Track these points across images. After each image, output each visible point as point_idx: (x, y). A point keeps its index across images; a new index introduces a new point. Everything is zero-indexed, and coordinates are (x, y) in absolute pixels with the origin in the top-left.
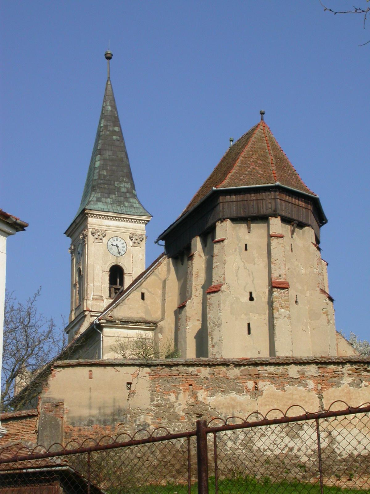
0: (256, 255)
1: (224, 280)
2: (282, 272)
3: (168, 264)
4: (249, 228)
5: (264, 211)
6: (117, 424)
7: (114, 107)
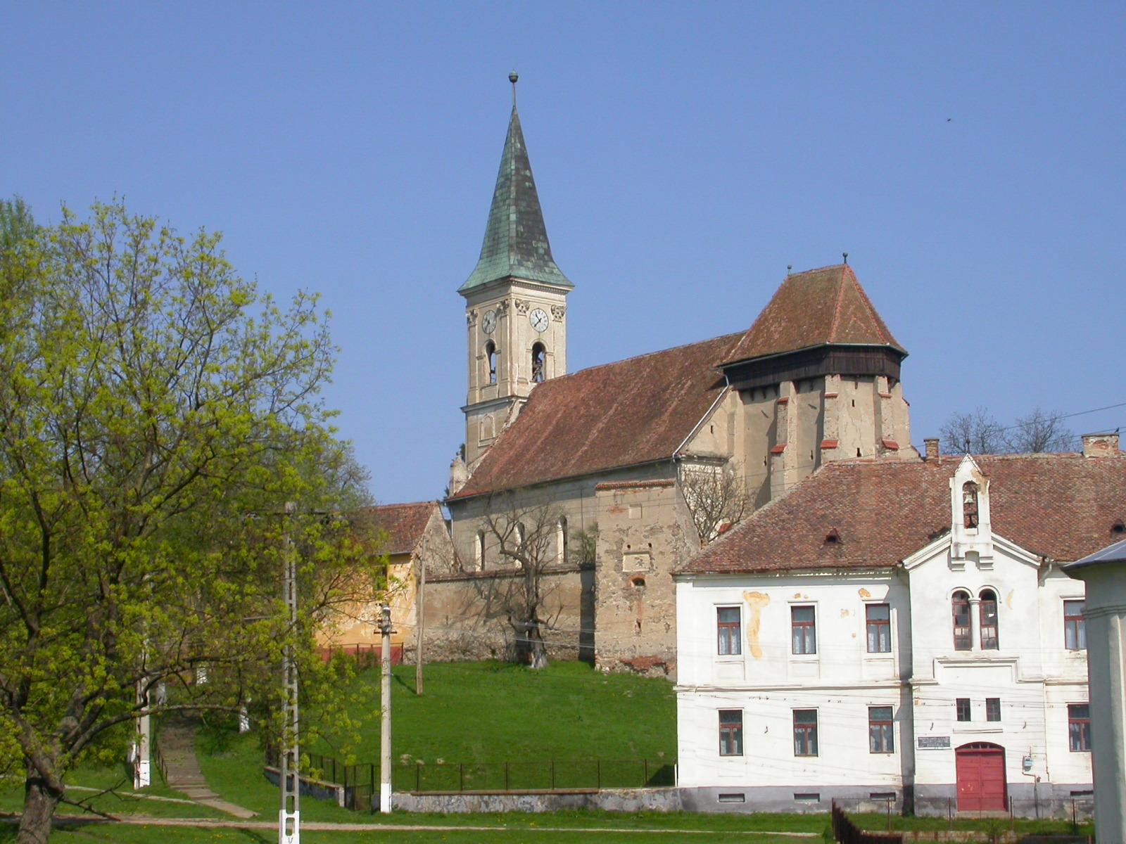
0: (863, 412)
1: (838, 435)
2: (890, 432)
3: (733, 398)
4: (856, 385)
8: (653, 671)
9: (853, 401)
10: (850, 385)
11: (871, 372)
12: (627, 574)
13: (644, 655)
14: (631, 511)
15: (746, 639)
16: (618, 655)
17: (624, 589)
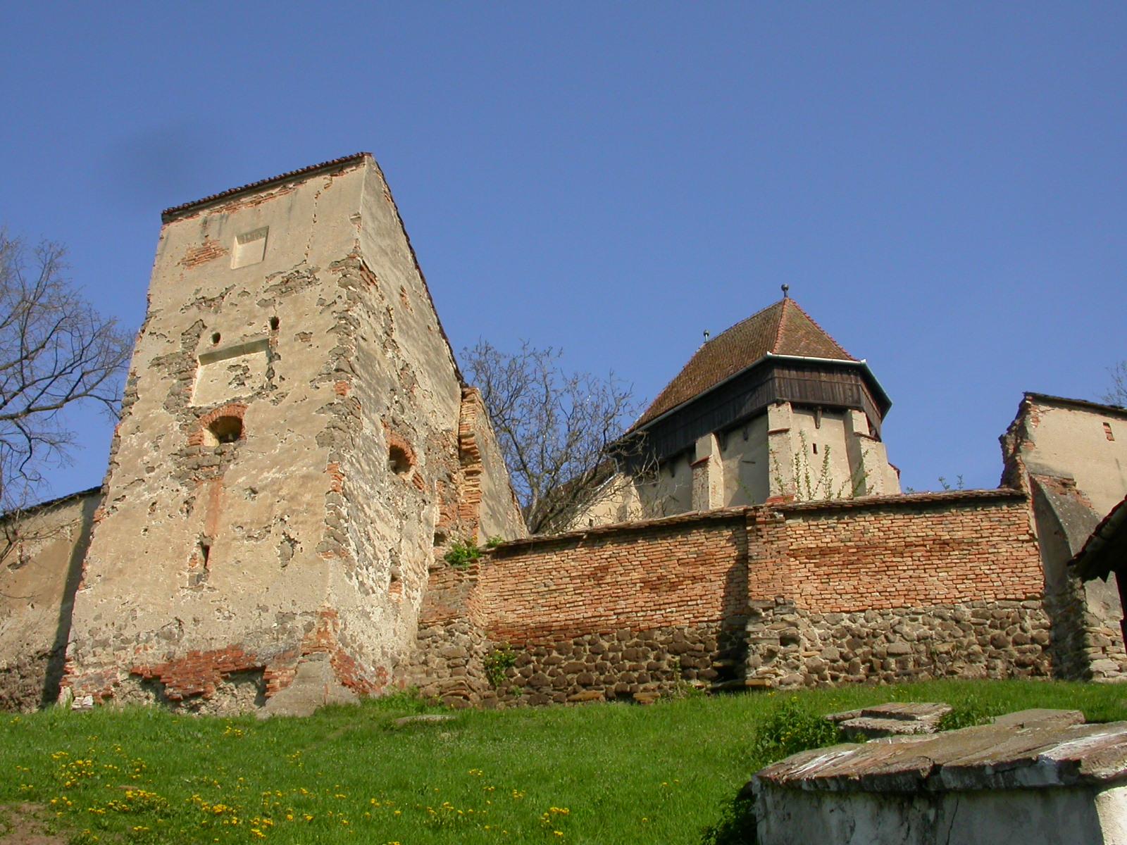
8: (226, 702)
9: (814, 445)
10: (806, 421)
11: (840, 401)
12: (197, 413)
13: (202, 648)
14: (238, 250)
15: (403, 248)
16: (128, 655)
17: (181, 453)
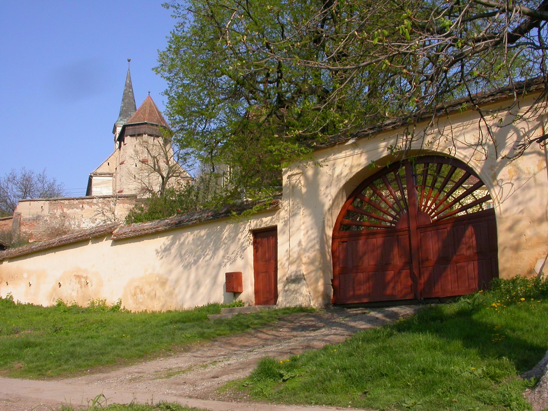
5: (141, 132)
6: (38, 220)
7: (130, 81)
